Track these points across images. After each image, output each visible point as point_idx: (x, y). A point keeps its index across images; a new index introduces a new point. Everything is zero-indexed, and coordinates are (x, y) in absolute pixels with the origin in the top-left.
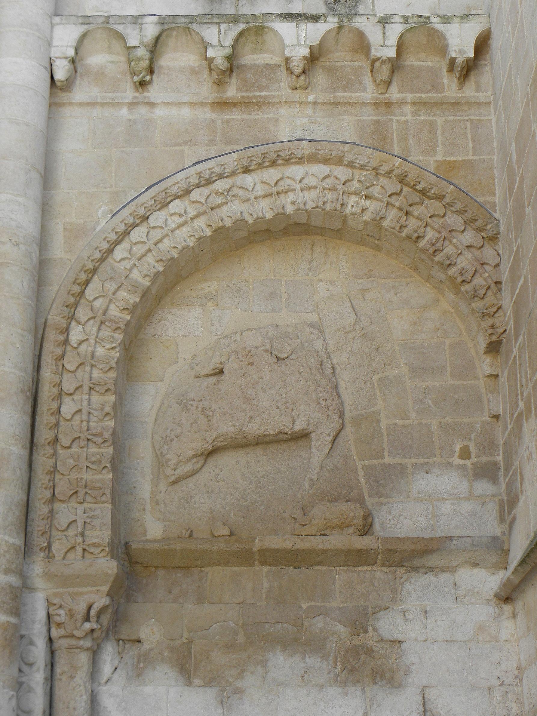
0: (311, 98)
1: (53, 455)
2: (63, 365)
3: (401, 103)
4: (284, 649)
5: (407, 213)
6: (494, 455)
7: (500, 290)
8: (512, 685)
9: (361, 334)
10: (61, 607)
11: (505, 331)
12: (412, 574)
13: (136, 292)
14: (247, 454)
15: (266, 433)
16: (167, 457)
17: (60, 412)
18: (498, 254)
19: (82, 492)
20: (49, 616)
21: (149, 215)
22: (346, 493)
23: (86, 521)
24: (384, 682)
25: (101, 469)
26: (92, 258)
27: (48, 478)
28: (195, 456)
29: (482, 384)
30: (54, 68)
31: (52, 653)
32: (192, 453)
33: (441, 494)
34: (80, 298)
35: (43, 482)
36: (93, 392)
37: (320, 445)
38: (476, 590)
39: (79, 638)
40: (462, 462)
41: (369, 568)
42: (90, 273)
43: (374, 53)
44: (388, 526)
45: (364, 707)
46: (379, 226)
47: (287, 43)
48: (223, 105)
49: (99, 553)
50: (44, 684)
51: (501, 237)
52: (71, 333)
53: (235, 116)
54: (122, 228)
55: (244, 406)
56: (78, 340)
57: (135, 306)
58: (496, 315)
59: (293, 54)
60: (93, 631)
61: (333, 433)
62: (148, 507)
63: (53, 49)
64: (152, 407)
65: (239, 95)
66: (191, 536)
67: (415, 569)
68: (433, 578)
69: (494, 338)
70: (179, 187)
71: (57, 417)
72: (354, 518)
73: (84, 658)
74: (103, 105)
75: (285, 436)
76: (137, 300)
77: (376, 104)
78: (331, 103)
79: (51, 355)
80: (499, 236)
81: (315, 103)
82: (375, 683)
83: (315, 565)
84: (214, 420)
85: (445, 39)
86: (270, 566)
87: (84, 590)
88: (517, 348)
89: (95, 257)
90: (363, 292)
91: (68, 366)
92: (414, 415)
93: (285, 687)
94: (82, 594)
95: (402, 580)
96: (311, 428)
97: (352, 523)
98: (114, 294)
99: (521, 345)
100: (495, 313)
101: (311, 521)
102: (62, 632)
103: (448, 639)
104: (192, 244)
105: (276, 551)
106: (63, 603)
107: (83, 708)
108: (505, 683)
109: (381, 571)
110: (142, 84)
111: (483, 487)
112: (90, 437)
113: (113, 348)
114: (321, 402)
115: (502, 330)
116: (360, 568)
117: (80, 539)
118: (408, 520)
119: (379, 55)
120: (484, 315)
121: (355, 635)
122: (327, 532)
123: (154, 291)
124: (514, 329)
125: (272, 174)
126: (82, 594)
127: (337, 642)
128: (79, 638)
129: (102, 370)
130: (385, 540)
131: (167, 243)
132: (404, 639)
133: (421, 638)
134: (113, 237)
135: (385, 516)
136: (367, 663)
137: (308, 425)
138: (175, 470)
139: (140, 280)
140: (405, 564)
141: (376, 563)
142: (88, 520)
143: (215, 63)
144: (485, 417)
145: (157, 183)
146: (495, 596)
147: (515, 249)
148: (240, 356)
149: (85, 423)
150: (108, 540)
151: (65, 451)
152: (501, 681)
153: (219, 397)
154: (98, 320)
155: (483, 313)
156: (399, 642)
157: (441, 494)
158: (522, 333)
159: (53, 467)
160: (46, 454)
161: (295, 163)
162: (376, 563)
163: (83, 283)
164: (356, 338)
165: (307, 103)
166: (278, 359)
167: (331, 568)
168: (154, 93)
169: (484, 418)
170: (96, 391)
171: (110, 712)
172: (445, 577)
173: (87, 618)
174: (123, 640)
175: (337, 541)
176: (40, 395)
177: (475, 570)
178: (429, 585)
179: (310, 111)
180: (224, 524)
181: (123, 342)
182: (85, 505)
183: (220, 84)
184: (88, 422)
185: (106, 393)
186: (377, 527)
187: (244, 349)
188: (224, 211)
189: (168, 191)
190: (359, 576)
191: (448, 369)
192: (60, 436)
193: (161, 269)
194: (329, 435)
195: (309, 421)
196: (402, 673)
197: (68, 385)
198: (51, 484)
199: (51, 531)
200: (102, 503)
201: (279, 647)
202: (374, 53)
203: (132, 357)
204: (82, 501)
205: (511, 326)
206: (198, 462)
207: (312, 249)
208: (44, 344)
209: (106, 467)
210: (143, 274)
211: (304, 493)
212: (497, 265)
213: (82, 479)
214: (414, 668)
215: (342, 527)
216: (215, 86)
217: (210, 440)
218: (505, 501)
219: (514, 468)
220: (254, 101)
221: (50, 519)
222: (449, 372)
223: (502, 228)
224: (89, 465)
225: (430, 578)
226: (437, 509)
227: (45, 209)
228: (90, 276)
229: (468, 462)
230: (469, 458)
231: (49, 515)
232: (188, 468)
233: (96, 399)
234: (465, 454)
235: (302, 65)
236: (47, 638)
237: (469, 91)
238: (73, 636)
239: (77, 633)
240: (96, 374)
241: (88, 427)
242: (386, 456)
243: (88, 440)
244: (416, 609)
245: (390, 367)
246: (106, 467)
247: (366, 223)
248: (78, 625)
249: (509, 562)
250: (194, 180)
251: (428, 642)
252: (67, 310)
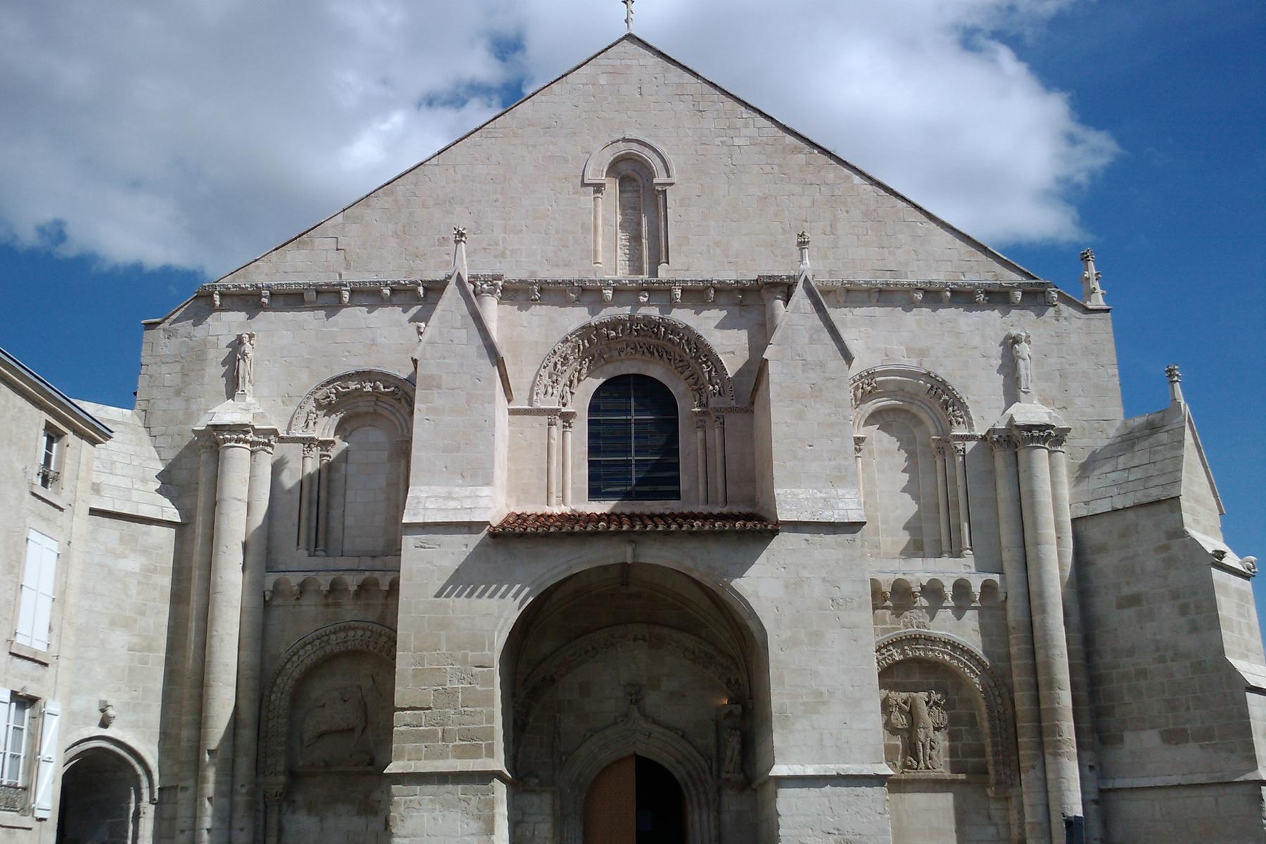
53: (331, 610)
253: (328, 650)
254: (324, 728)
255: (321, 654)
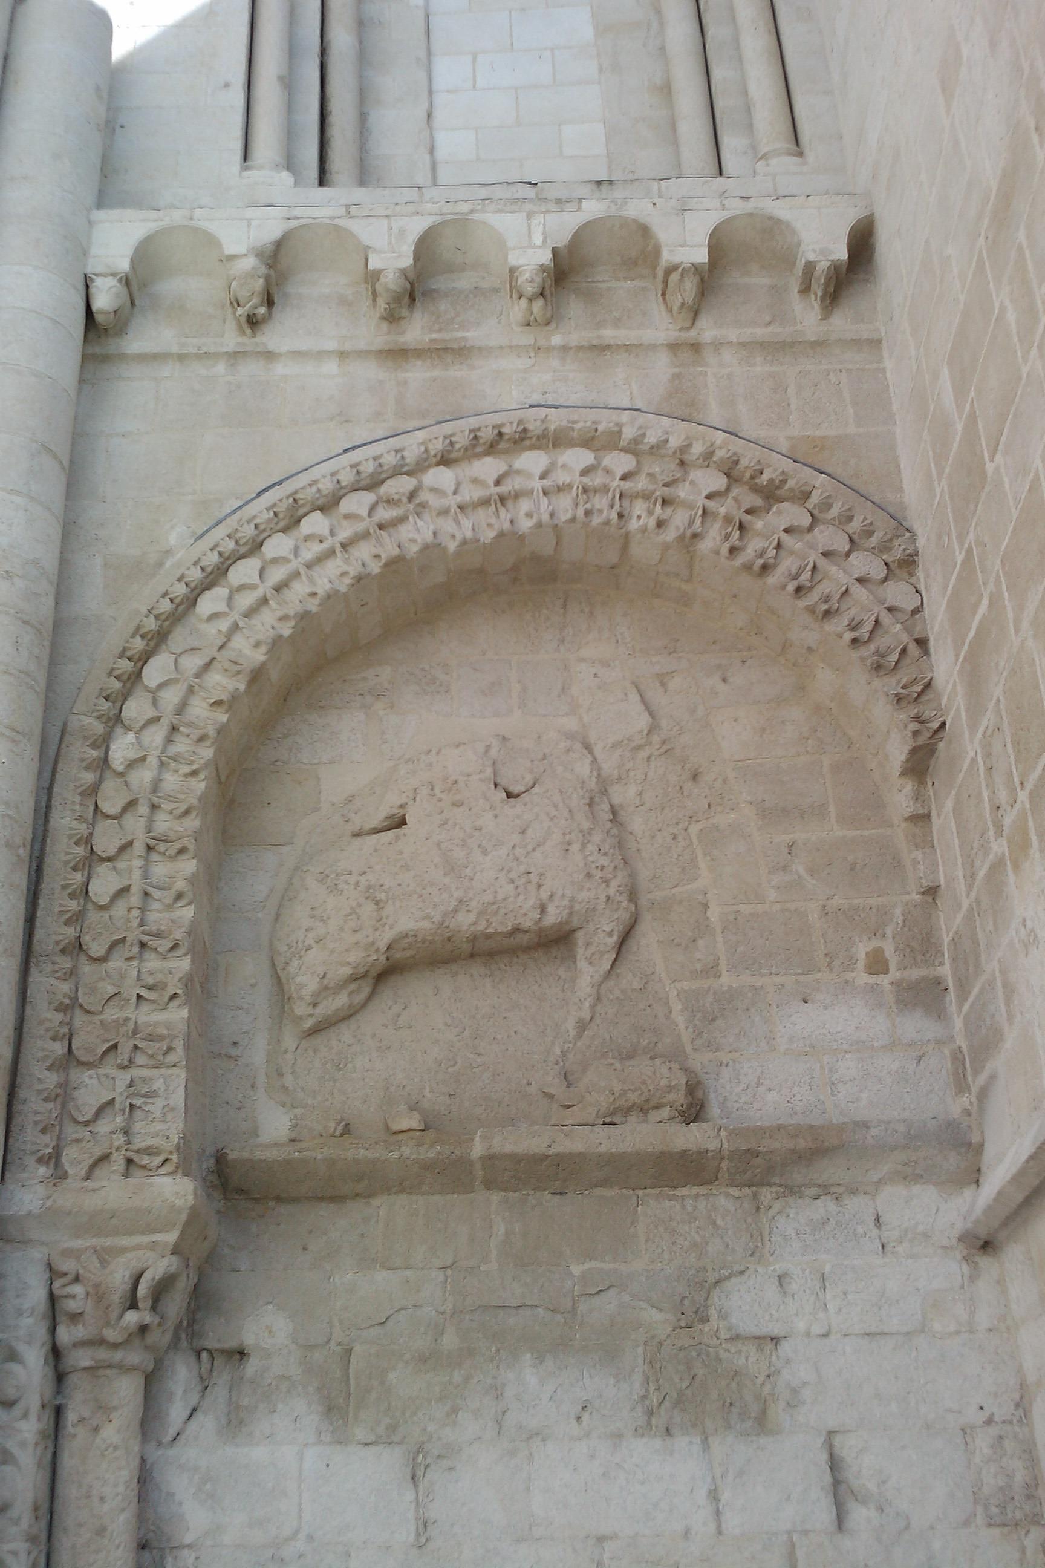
0: (556, 340)
1: (71, 974)
2: (96, 805)
3: (717, 345)
4: (540, 1359)
5: (741, 527)
6: (933, 965)
7: (926, 652)
8: (1011, 1422)
9: (662, 750)
10: (77, 1279)
11: (943, 724)
12: (791, 1200)
13: (239, 672)
14: (455, 974)
15: (491, 930)
16: (298, 980)
17: (87, 892)
18: (917, 591)
19: (125, 1050)
20: (52, 1299)
21: (265, 539)
22: (649, 1043)
23: (134, 1102)
24: (748, 1424)
25: (166, 999)
26: (155, 612)
27: (60, 1016)
28: (354, 978)
29: (900, 833)
30: (93, 290)
31: (60, 1378)
32: (347, 971)
33: (835, 1041)
34: (133, 684)
35: (48, 1025)
36: (154, 857)
37: (593, 954)
38: (921, 1228)
39: (115, 1346)
40: (872, 979)
41: (703, 1190)
42: (152, 638)
43: (667, 257)
44: (736, 1106)
45: (709, 1479)
46: (689, 552)
47: (510, 243)
48: (398, 355)
49: (158, 1167)
50: (37, 1444)
51: (921, 560)
52: (113, 747)
53: (417, 374)
54: (213, 559)
55: (447, 880)
56: (126, 759)
57: (235, 697)
58: (924, 698)
59: (521, 262)
60: (143, 1329)
61: (619, 929)
62: (261, 1080)
63: (91, 261)
64: (271, 890)
65: (427, 338)
66: (347, 1131)
67: (792, 1191)
68: (832, 1207)
69: (922, 740)
70: (319, 490)
71: (82, 902)
72: (670, 1088)
73: (126, 1391)
74: (181, 358)
75: (526, 937)
76: (242, 687)
77: (674, 347)
78: (592, 348)
79: (72, 785)
80: (916, 558)
81: (565, 349)
82: (728, 1427)
83: (596, 1186)
84: (389, 909)
85: (794, 232)
86: (505, 1190)
87: (126, 1241)
88: (977, 741)
89: (162, 611)
90: (663, 679)
91: (106, 807)
92: (772, 895)
93: (544, 1440)
94: (123, 1250)
95: (771, 1213)
96: (575, 923)
97: (665, 1100)
98: (198, 676)
99: (989, 733)
100: (920, 695)
101: (583, 1097)
102: (80, 1332)
103: (873, 1329)
104: (343, 589)
105: (516, 1159)
106: (81, 1271)
107: (120, 1497)
108: (996, 1419)
109: (728, 1195)
110: (253, 322)
111: (915, 1025)
112: (145, 938)
113: (194, 773)
114: (594, 872)
115: (935, 725)
116: (684, 1191)
117: (120, 1140)
118: (774, 1093)
119: (677, 259)
120: (899, 699)
121: (681, 1328)
122: (616, 1119)
123: (274, 674)
124: (967, 710)
125: (488, 467)
126: (123, 1250)
127: (646, 1343)
128: (115, 1346)
129: (171, 813)
130: (734, 1133)
131: (300, 588)
132: (782, 1334)
133: (817, 1329)
134: (196, 574)
135: (728, 1087)
136: (705, 1386)
137: (571, 913)
138: (315, 1005)
139: (248, 651)
140: (776, 1179)
141: (717, 1179)
142: (138, 1102)
143: (382, 279)
144: (908, 893)
145: (279, 483)
146: (959, 1240)
147: (960, 558)
148: (437, 791)
149: (135, 913)
150: (176, 1140)
151: (95, 966)
152: (987, 1414)
153: (399, 865)
154: (165, 723)
155: (896, 695)
156: (772, 1339)
157: (835, 1041)
158: (991, 705)
159: (70, 998)
160: (56, 972)
161: (532, 448)
162: (717, 1179)
163: (137, 656)
164: (653, 758)
165: (549, 349)
166: (509, 795)
167: (625, 1191)
168: (273, 337)
169: (907, 897)
170: (159, 853)
171: (180, 1504)
172: (853, 1204)
173: (133, 1305)
174: (209, 1351)
175: (638, 1136)
176: (48, 860)
177: (916, 1189)
178: (825, 1222)
179: (555, 363)
180: (412, 1109)
181: (215, 762)
182: (135, 1072)
183: (392, 318)
184: (143, 910)
185: (181, 857)
186: (714, 1110)
187: (445, 779)
188: (405, 532)
189: (297, 496)
190: (683, 1207)
191: (832, 808)
192: (86, 939)
193: (287, 632)
194: (610, 934)
195: (571, 907)
196: (782, 1404)
197: (106, 841)
198: (65, 1030)
199: (61, 1123)
200: (168, 1067)
201: (528, 1356)
202: (667, 257)
203: (232, 801)
204: (126, 1063)
205: (958, 709)
206: (359, 990)
207: (564, 606)
208: (60, 766)
209: (174, 996)
210: (252, 641)
211: (567, 1045)
212: (916, 611)
213: (127, 1019)
214: (806, 1394)
215: (644, 1109)
216: (385, 326)
217: (382, 945)
218: (965, 1049)
219: (983, 978)
220: (455, 346)
221: (60, 1099)
222: (833, 815)
223: (921, 543)
224: (144, 993)
225: (825, 1206)
226: (830, 1070)
227: (70, 530)
228: (152, 644)
229: (885, 980)
230: (887, 972)
231: (59, 1091)
232: (341, 1001)
233: (160, 869)
234: (877, 964)
235: (538, 280)
236: (47, 1347)
237: (841, 323)
238: (101, 1342)
239: (111, 1335)
240: (163, 823)
241: (142, 919)
242: (724, 973)
243: (143, 945)
244: (804, 1271)
245: (720, 809)
246: (174, 996)
247: (666, 547)
248: (114, 1315)
249: (984, 1169)
250: (347, 478)
251: (832, 1337)
252: (106, 705)
253: (416, 534)
254: (408, 919)
255: (367, 557)
